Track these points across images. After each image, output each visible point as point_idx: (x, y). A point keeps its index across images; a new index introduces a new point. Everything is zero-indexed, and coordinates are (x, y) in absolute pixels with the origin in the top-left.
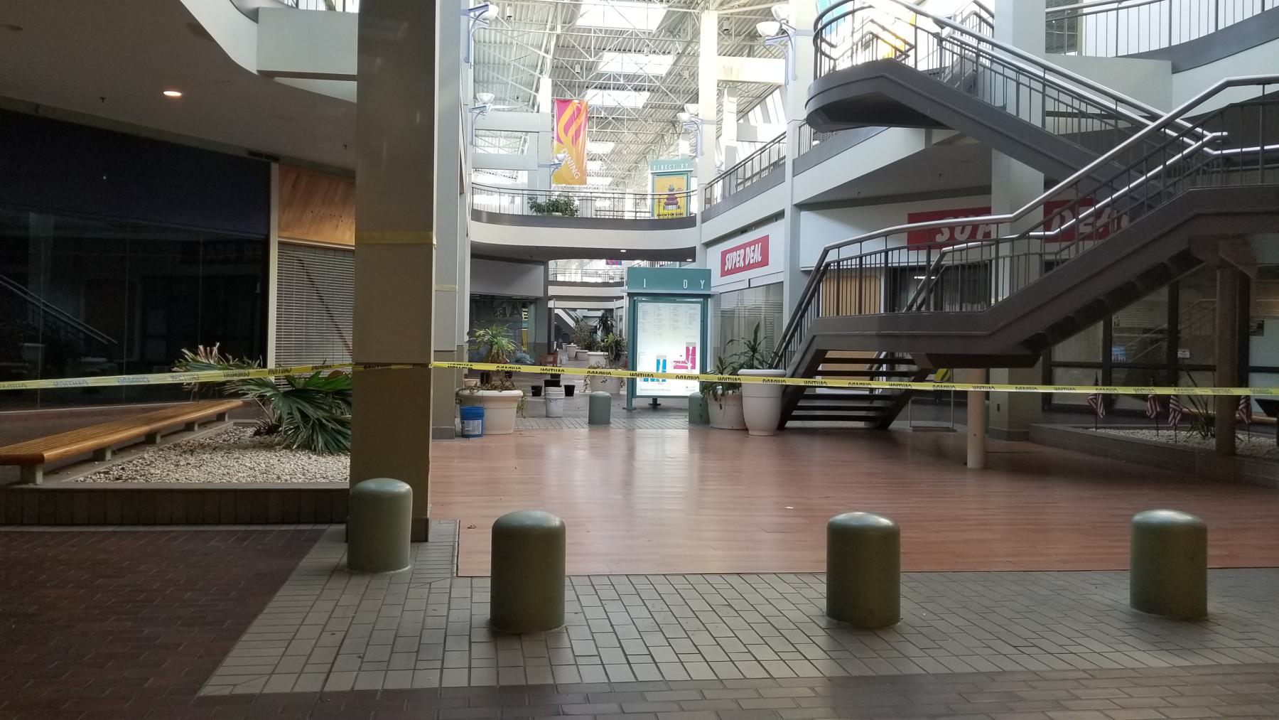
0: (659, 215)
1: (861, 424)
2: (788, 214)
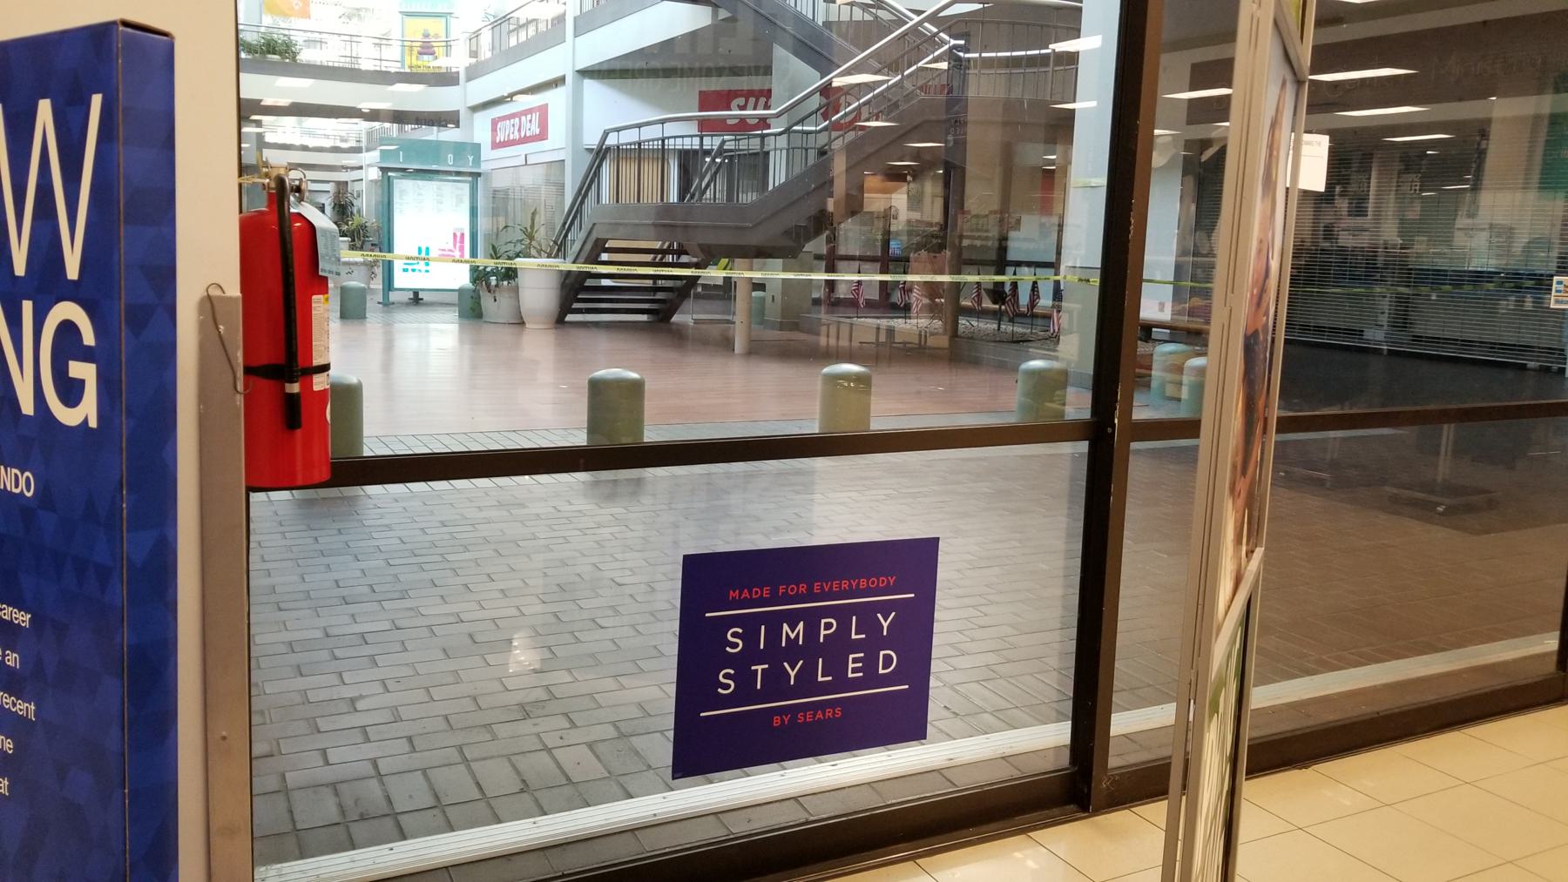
0: (411, 67)
1: (644, 318)
2: (569, 80)
